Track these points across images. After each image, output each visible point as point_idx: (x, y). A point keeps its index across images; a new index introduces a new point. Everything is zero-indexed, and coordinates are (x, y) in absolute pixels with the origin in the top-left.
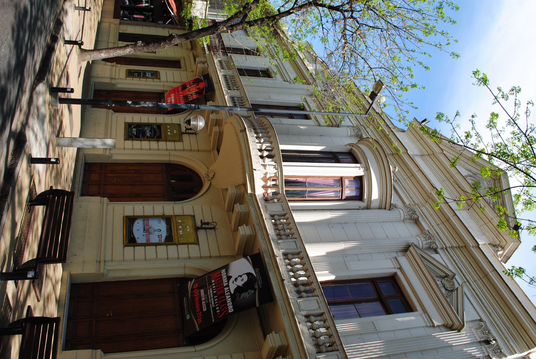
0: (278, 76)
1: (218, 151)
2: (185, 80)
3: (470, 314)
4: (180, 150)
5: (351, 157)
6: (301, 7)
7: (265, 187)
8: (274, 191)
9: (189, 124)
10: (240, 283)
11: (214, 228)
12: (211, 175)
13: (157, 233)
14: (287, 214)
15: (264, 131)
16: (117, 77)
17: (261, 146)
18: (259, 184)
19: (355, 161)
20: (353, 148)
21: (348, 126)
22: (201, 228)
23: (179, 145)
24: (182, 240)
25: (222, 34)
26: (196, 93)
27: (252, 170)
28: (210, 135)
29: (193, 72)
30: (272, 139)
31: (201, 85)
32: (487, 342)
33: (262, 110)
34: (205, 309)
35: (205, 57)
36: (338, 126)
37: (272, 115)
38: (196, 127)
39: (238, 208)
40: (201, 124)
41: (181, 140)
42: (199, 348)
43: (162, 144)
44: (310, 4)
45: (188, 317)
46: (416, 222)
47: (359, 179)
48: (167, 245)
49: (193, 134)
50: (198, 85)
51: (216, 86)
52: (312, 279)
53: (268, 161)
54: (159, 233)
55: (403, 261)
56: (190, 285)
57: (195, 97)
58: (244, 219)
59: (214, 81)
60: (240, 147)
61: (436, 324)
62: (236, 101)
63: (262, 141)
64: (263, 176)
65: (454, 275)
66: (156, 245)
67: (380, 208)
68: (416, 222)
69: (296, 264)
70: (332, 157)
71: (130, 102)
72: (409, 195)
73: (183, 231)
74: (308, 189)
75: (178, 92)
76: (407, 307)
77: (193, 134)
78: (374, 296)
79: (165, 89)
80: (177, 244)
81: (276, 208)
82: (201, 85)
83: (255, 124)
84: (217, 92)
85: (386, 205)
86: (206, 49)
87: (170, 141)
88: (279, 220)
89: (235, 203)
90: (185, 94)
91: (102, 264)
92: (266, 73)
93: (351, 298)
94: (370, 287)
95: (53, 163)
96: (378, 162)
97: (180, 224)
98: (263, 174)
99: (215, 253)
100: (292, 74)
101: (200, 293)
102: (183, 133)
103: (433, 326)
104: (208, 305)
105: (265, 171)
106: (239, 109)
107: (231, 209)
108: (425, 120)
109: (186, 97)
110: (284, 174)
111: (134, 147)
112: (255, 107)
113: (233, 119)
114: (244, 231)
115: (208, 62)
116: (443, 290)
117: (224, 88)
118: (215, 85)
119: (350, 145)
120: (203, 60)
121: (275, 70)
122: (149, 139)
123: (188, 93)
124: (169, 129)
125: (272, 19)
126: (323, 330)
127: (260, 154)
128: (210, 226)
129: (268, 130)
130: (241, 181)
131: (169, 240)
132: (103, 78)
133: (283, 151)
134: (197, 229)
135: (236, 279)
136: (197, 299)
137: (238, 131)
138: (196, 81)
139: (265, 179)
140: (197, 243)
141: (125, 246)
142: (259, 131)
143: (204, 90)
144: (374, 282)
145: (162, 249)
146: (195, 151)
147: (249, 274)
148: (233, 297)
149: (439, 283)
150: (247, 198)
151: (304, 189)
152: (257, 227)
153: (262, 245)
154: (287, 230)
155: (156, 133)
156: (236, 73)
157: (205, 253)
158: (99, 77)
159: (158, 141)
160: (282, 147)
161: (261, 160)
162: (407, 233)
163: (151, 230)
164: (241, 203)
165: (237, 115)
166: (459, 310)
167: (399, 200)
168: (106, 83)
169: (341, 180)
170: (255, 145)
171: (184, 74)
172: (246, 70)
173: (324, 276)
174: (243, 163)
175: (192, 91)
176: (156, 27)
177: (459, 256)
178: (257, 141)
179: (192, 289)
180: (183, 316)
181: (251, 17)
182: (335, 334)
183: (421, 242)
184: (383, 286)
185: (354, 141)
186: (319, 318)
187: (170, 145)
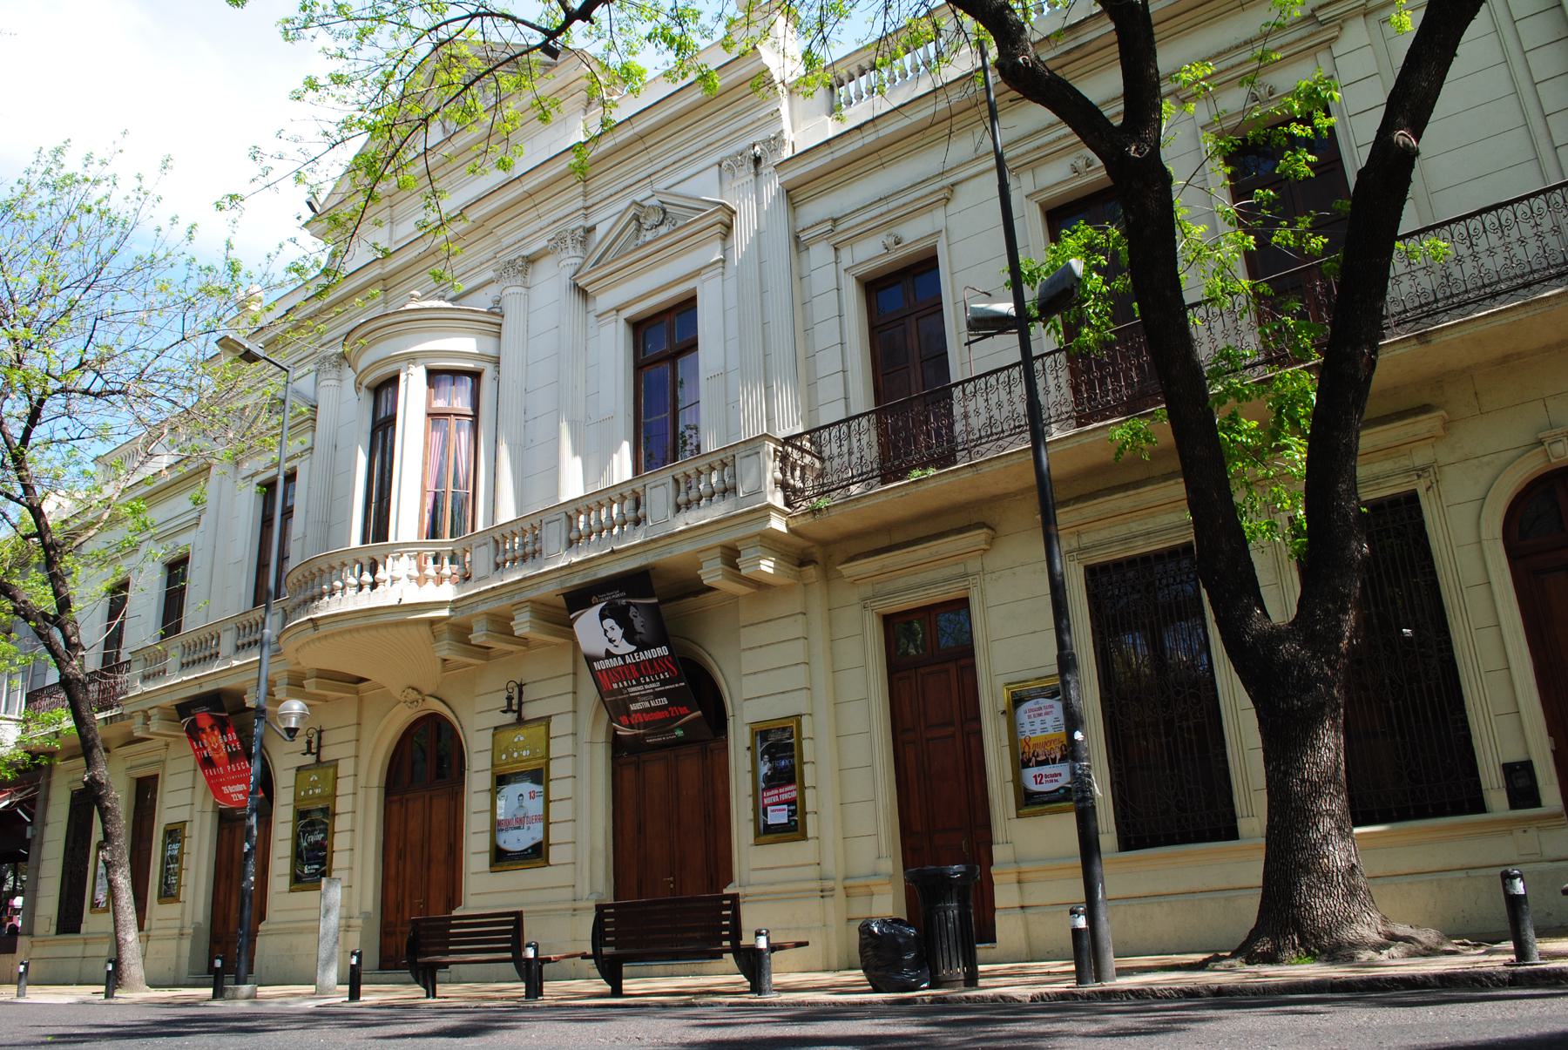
0: (183, 540)
1: (362, 680)
2: (190, 761)
3: (705, 187)
4: (356, 765)
5: (385, 388)
6: (27, 488)
7: (440, 580)
8: (446, 561)
9: (295, 730)
10: (617, 633)
11: (520, 686)
12: (414, 695)
13: (527, 802)
14: (498, 538)
15: (317, 581)
16: (178, 923)
17: (352, 586)
18: (431, 593)
19: (393, 381)
20: (365, 382)
21: (316, 383)
22: (519, 712)
23: (345, 768)
24: (541, 751)
25: (88, 671)
26: (223, 733)
27: (401, 607)
28: (325, 699)
29: (167, 745)
30: (336, 563)
31: (205, 722)
32: (757, 161)
33: (272, 583)
34: (664, 701)
35: (130, 717)
36: (314, 408)
37: (283, 558)
38: (302, 716)
39: (478, 637)
40: (296, 706)
41: (334, 764)
42: (730, 712)
43: (342, 805)
44: (19, 462)
45: (679, 733)
46: (531, 260)
47: (433, 375)
48: (548, 780)
49: (320, 739)
50: (203, 730)
51: (207, 688)
52: (627, 491)
53: (381, 574)
54: (526, 796)
55: (604, 301)
56: (624, 732)
57: (233, 736)
58: (501, 624)
59: (195, 691)
60: (350, 631)
61: (719, 256)
62: (246, 640)
63: (338, 584)
64: (414, 584)
65: (634, 202)
66: (547, 802)
67: (499, 335)
68: (531, 260)
69: (588, 524)
70: (383, 429)
71: (247, 846)
72: (474, 265)
73: (524, 748)
74: (450, 488)
75: (218, 776)
76: (686, 306)
77: (320, 739)
78: (667, 366)
79: (209, 807)
80: (548, 760)
81: (481, 560)
82: (205, 722)
83: (302, 597)
84: (223, 684)
85: (494, 323)
86: (108, 714)
87: (335, 788)
88: (505, 551)
89: (468, 643)
90: (226, 759)
91: (579, 905)
92: (176, 569)
93: (668, 415)
94: (654, 372)
95: (359, 961)
96: (399, 333)
97: (509, 755)
98: (411, 583)
99: (566, 684)
100: (181, 504)
101: (636, 711)
102: (318, 760)
103: (724, 261)
104: (657, 695)
105: (405, 580)
106: (267, 631)
107: (484, 651)
108: (310, 204)
109: (233, 757)
110: (415, 540)
111: (346, 865)
112: (261, 595)
113: (289, 646)
114: (523, 624)
115: (145, 707)
116: (663, 230)
117: (216, 668)
118: (206, 688)
119: (357, 389)
120: (139, 719)
121: (170, 544)
122: (328, 832)
123: (223, 753)
124: (306, 792)
125: (49, 549)
126: (714, 478)
127: (367, 589)
128: (516, 695)
129: (315, 570)
130: (425, 630)
131: (539, 776)
132: (178, 957)
133: (365, 540)
134: (520, 721)
135: (611, 641)
136: (647, 717)
137: (316, 634)
138: (194, 733)
139: (421, 580)
140: (546, 720)
141: (547, 863)
142: (317, 591)
143: (220, 718)
144: (642, 365)
145: (556, 790)
146: (359, 733)
147: (602, 617)
148: (642, 647)
149: (649, 236)
150: (459, 618)
151: (450, 496)
152: (516, 599)
153: (549, 591)
154: (520, 541)
155: (315, 824)
156: (175, 641)
157: (566, 703)
158: (178, 964)
159: (334, 815)
160: (355, 541)
161: (380, 587)
162: (551, 281)
163: (520, 815)
164: (470, 630)
165: (278, 638)
166: (698, 207)
167: (486, 289)
168: (192, 949)
169: (434, 416)
170: (348, 600)
171: (171, 767)
172: (165, 620)
173: (622, 466)
174: (386, 625)
175: (217, 743)
176: (41, 844)
177: (605, 183)
178: (338, 595)
179: (632, 727)
180: (678, 743)
181: (49, 604)
182: (722, 455)
183: (570, 259)
184: (652, 350)
185: (350, 376)
186: (694, 483)
187: (344, 786)
